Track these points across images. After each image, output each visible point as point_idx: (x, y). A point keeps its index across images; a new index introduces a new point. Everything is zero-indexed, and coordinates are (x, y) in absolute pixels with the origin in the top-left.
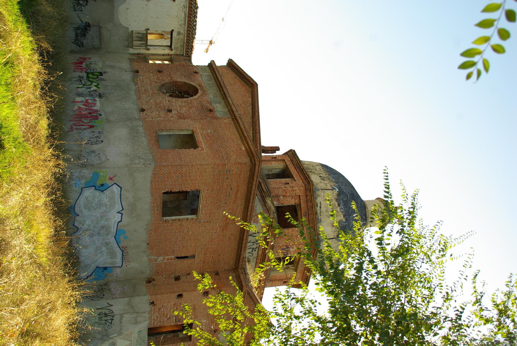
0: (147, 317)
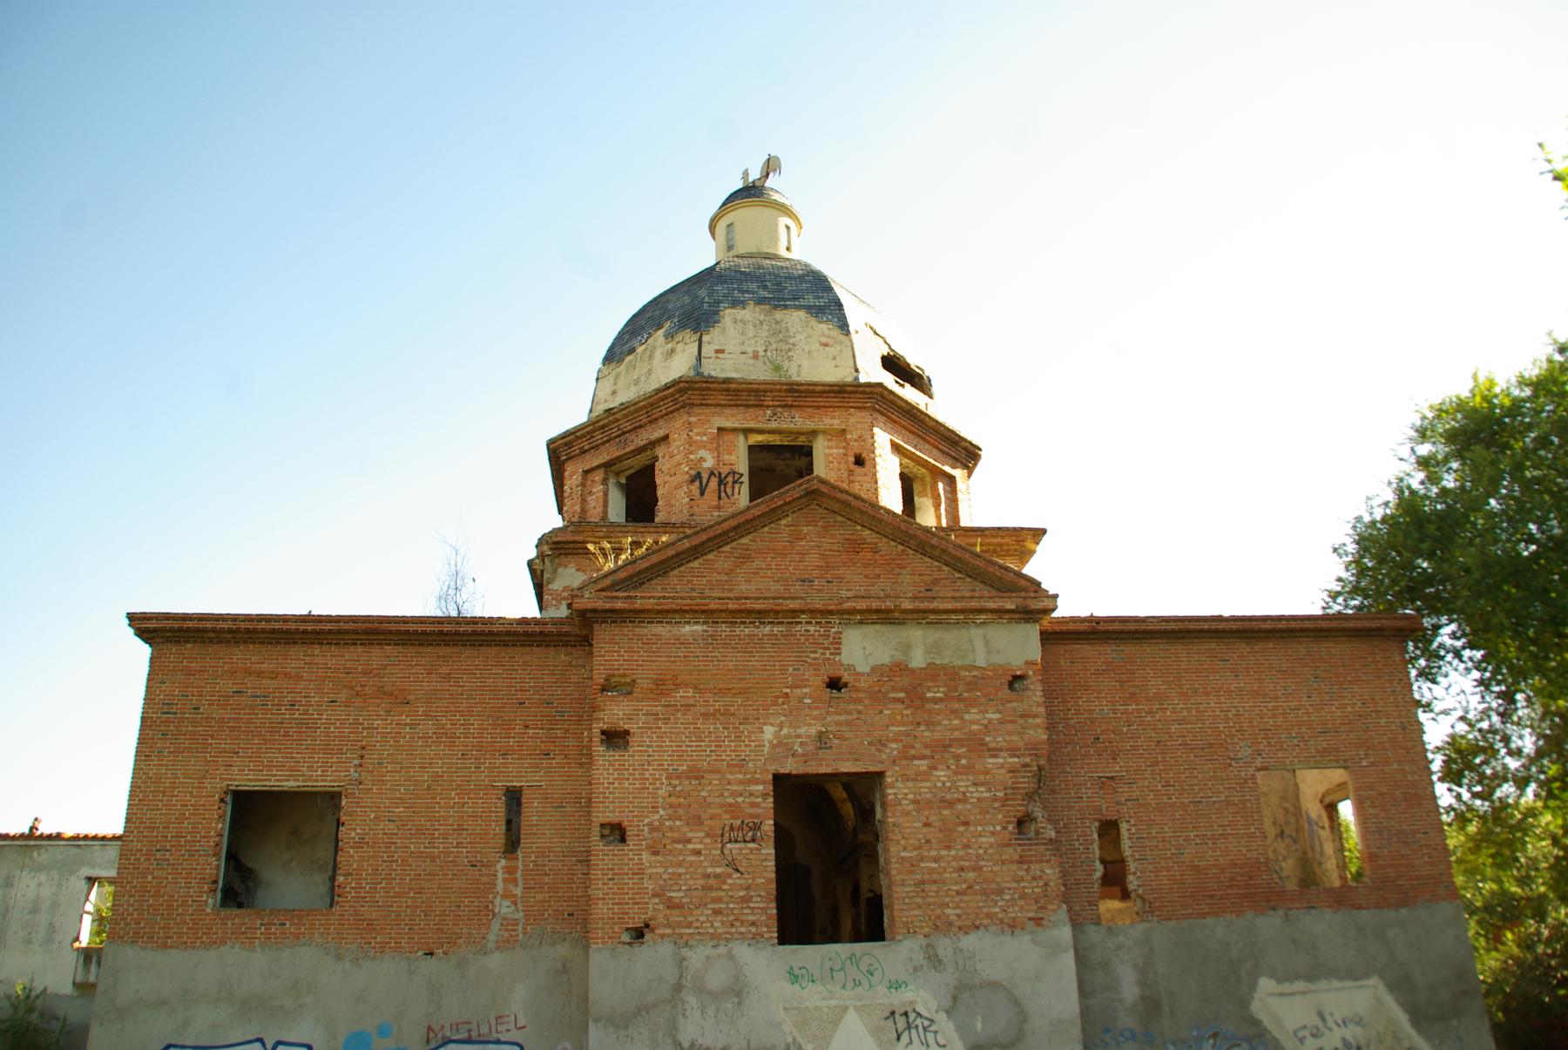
0: (710, 951)
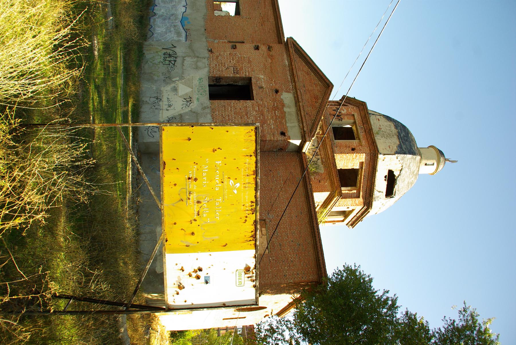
0: (206, 64)
